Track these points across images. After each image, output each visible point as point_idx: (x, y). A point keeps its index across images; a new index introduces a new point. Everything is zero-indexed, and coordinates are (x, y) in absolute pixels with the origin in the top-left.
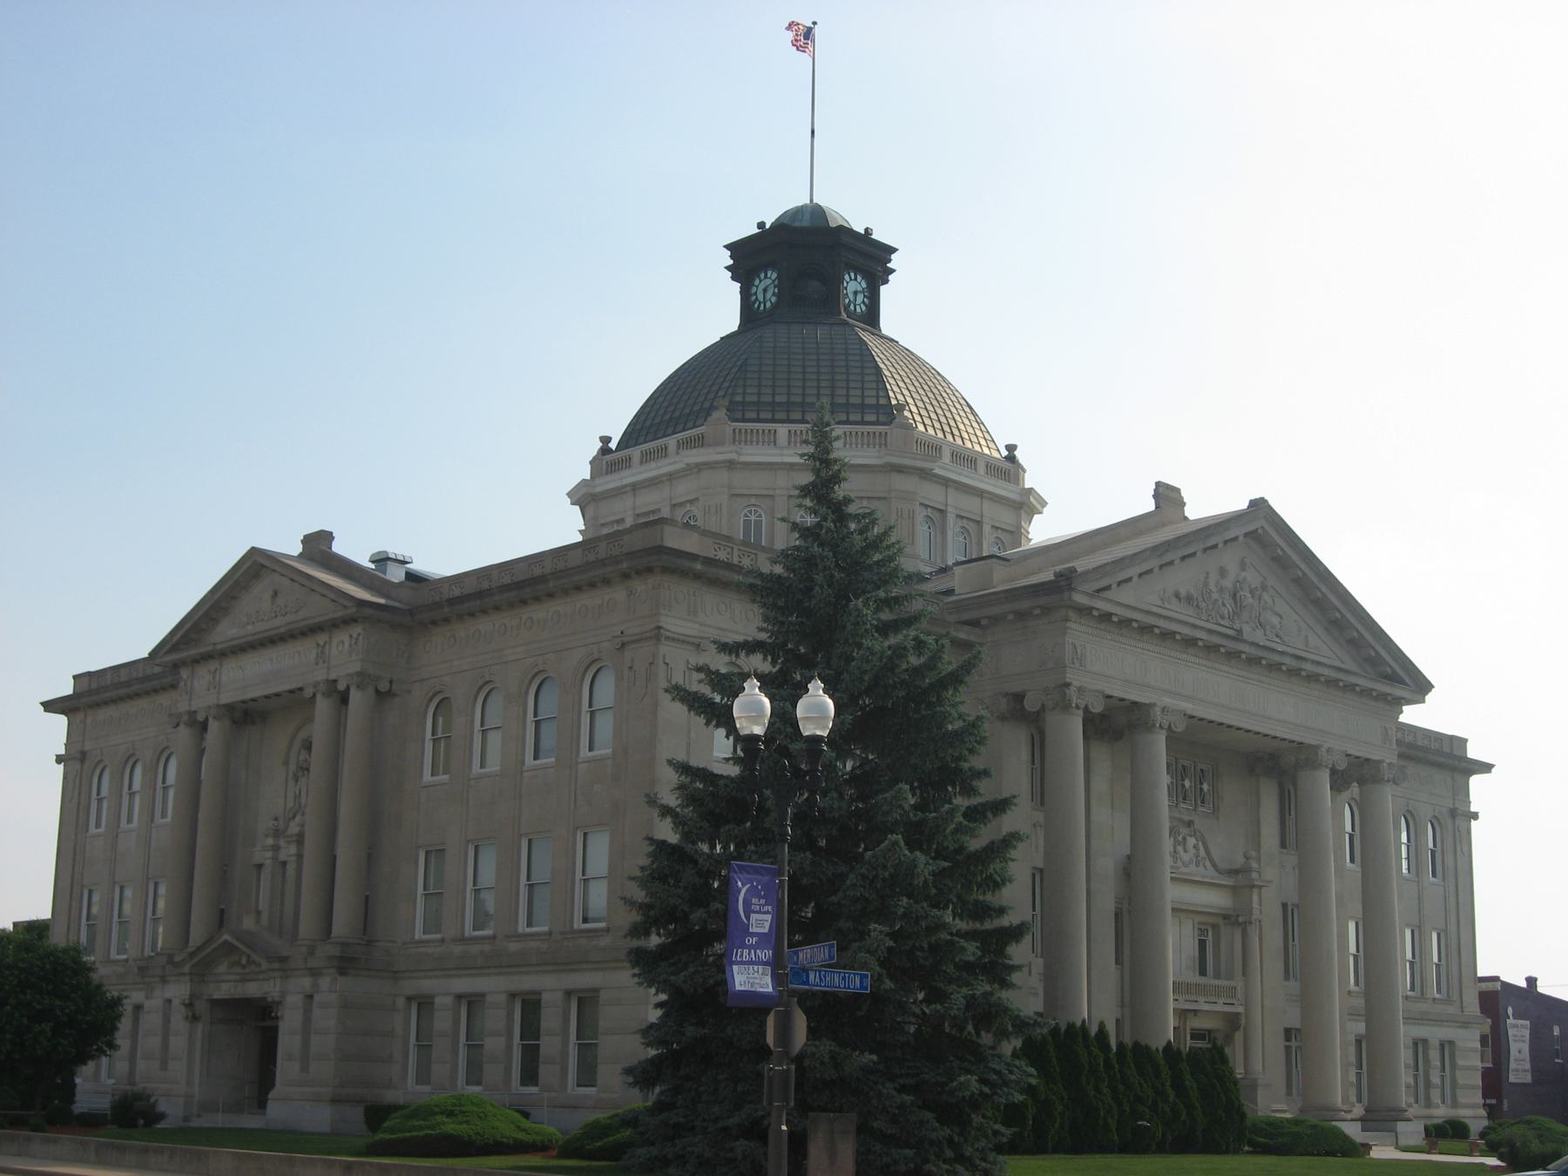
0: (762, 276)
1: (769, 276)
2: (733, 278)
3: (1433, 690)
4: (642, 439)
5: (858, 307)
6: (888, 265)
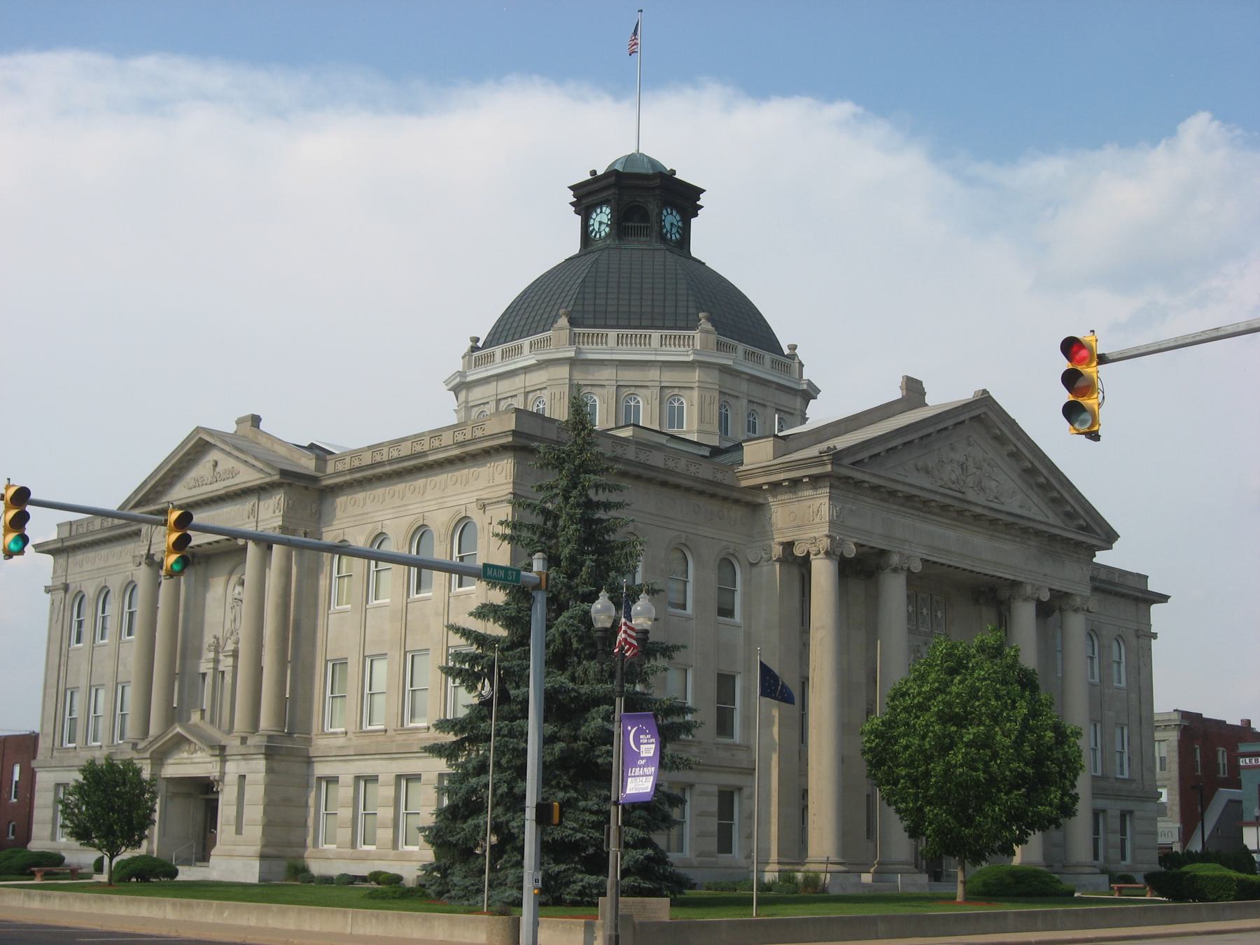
0: (598, 211)
1: (603, 211)
2: (577, 212)
3: (1119, 539)
4: (510, 338)
5: (673, 236)
6: (698, 203)
